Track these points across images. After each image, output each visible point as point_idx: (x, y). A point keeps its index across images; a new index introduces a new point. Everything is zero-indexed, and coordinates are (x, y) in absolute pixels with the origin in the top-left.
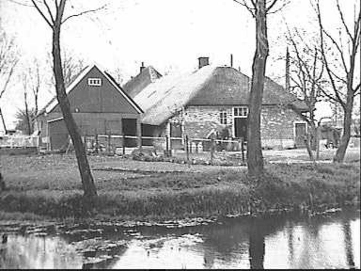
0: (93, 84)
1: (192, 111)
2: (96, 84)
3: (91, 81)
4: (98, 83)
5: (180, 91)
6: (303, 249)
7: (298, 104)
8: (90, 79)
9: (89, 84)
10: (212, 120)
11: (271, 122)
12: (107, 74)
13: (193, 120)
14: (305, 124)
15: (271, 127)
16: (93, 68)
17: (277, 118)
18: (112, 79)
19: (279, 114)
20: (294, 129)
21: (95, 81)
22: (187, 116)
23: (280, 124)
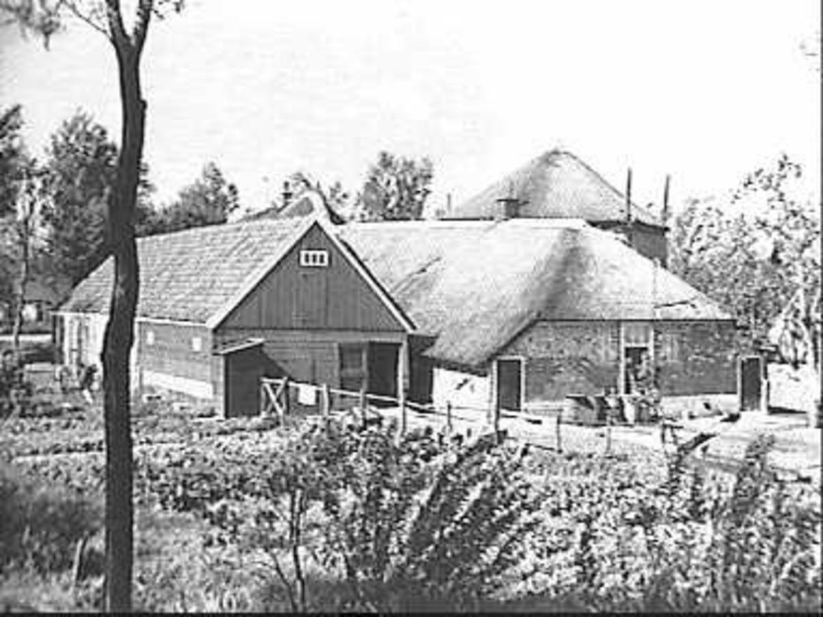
0: (311, 263)
1: (542, 332)
2: (318, 264)
3: (307, 256)
4: (307, 256)
5: (719, 448)
6: (551, 274)
7: (362, 492)
8: (303, 253)
9: (303, 262)
10: (581, 354)
11: (695, 357)
12: (345, 244)
13: (543, 353)
14: (757, 359)
15: (694, 368)
16: (312, 228)
17: (707, 347)
18: (350, 249)
19: (711, 339)
20: (738, 370)
21: (314, 257)
22: (533, 346)
23: (712, 360)
